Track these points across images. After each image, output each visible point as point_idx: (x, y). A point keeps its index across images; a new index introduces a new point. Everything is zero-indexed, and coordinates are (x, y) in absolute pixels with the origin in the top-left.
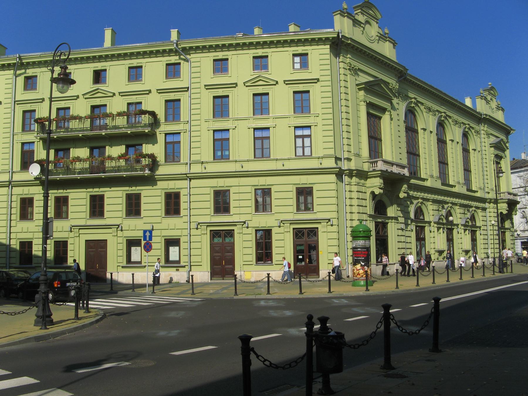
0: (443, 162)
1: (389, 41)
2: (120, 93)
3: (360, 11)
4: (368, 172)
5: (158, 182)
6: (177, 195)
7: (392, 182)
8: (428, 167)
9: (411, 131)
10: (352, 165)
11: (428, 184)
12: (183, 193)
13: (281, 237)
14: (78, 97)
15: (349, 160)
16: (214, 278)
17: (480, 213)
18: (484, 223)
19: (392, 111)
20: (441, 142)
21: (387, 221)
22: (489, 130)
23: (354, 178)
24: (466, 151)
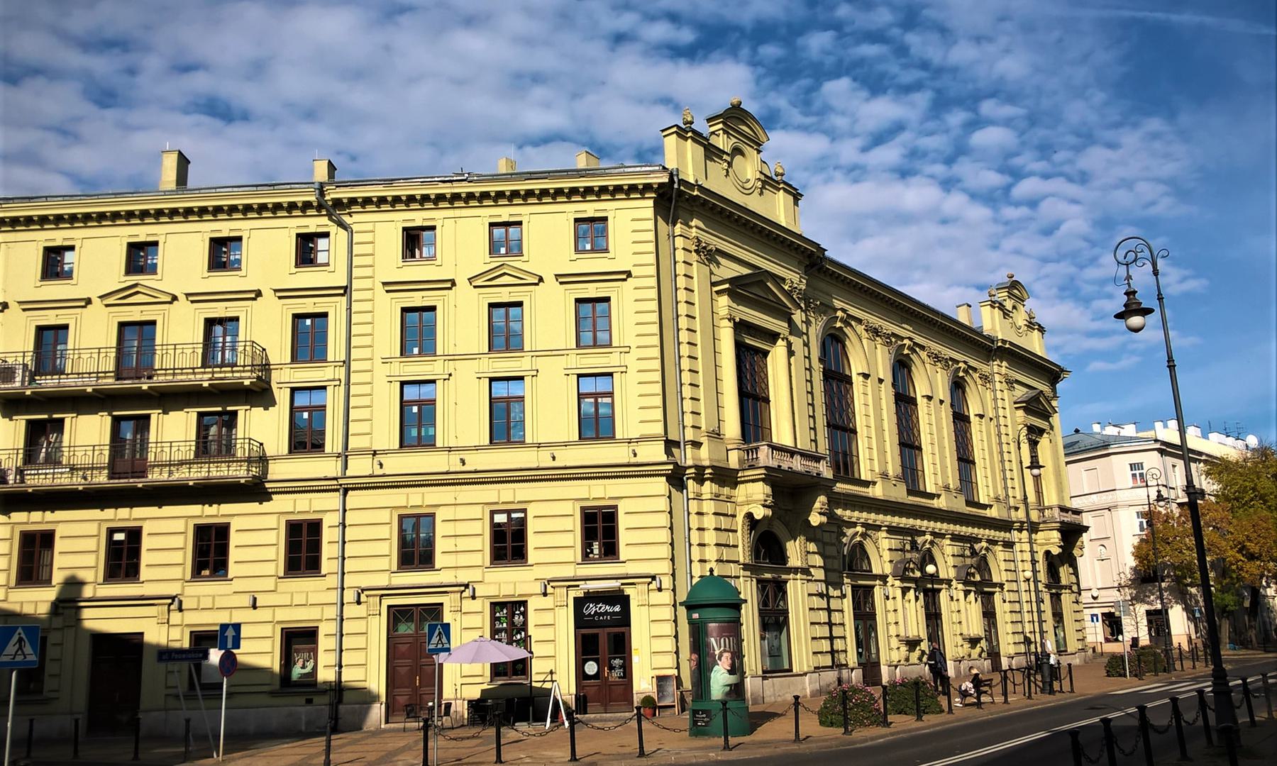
0: (909, 445)
1: (785, 190)
2: (187, 295)
3: (721, 126)
4: (738, 471)
5: (274, 497)
6: (315, 527)
7: (790, 491)
8: (875, 453)
9: (837, 380)
10: (704, 455)
11: (877, 492)
12: (330, 523)
13: (547, 618)
14: (89, 301)
15: (696, 445)
16: (395, 719)
17: (1000, 553)
18: (1011, 576)
19: (792, 338)
20: (905, 402)
21: (784, 577)
22: (1011, 373)
23: (707, 483)
24: (961, 419)
